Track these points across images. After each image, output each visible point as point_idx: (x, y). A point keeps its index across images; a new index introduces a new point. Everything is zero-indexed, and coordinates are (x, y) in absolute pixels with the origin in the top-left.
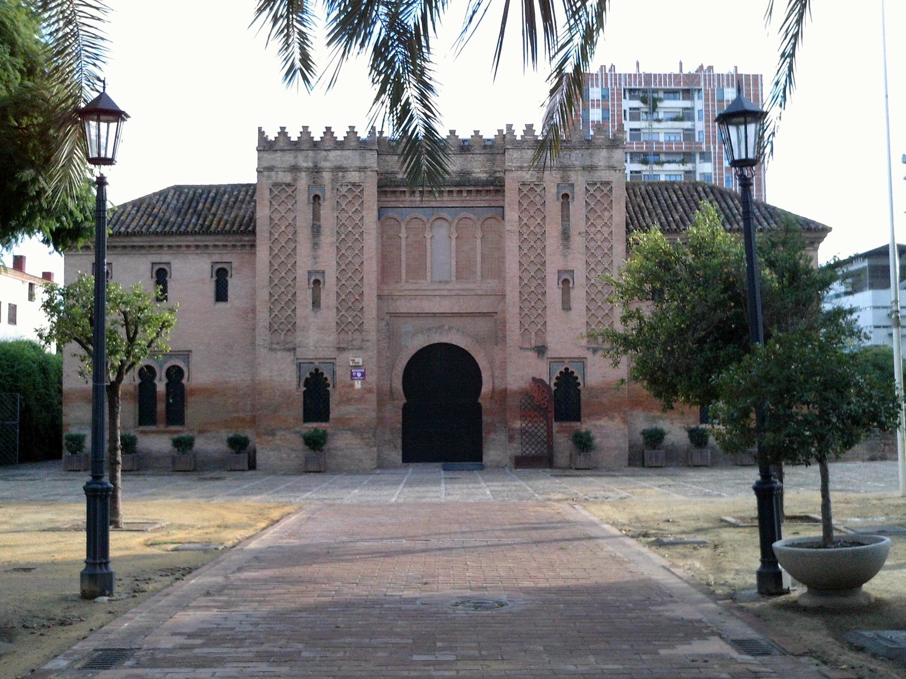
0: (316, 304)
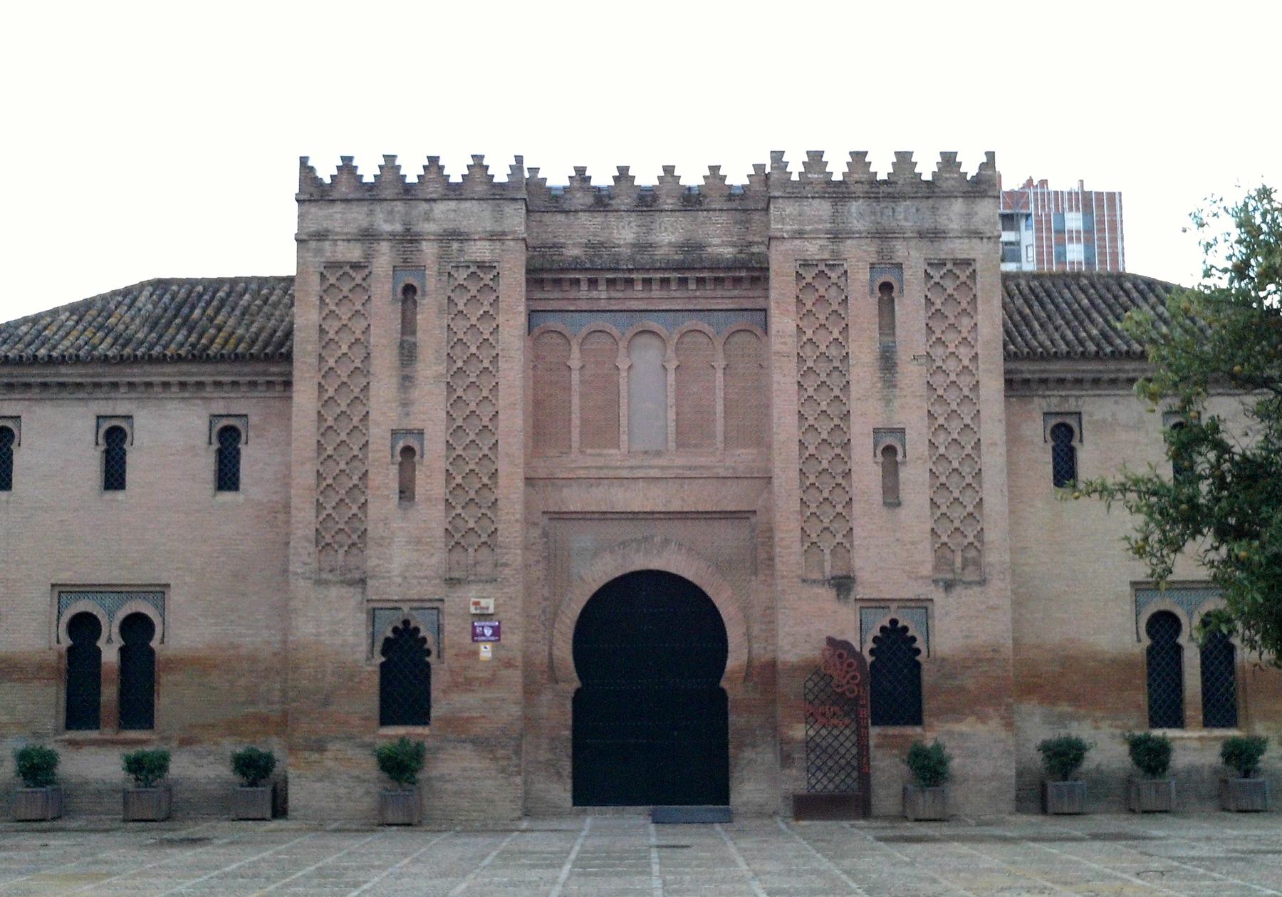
0: (406, 492)
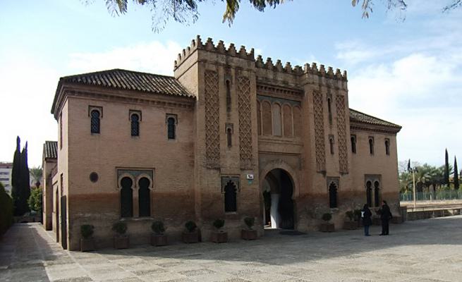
0: (230, 144)
